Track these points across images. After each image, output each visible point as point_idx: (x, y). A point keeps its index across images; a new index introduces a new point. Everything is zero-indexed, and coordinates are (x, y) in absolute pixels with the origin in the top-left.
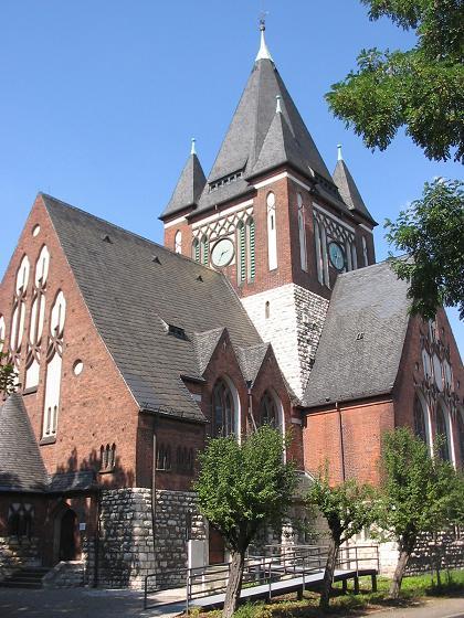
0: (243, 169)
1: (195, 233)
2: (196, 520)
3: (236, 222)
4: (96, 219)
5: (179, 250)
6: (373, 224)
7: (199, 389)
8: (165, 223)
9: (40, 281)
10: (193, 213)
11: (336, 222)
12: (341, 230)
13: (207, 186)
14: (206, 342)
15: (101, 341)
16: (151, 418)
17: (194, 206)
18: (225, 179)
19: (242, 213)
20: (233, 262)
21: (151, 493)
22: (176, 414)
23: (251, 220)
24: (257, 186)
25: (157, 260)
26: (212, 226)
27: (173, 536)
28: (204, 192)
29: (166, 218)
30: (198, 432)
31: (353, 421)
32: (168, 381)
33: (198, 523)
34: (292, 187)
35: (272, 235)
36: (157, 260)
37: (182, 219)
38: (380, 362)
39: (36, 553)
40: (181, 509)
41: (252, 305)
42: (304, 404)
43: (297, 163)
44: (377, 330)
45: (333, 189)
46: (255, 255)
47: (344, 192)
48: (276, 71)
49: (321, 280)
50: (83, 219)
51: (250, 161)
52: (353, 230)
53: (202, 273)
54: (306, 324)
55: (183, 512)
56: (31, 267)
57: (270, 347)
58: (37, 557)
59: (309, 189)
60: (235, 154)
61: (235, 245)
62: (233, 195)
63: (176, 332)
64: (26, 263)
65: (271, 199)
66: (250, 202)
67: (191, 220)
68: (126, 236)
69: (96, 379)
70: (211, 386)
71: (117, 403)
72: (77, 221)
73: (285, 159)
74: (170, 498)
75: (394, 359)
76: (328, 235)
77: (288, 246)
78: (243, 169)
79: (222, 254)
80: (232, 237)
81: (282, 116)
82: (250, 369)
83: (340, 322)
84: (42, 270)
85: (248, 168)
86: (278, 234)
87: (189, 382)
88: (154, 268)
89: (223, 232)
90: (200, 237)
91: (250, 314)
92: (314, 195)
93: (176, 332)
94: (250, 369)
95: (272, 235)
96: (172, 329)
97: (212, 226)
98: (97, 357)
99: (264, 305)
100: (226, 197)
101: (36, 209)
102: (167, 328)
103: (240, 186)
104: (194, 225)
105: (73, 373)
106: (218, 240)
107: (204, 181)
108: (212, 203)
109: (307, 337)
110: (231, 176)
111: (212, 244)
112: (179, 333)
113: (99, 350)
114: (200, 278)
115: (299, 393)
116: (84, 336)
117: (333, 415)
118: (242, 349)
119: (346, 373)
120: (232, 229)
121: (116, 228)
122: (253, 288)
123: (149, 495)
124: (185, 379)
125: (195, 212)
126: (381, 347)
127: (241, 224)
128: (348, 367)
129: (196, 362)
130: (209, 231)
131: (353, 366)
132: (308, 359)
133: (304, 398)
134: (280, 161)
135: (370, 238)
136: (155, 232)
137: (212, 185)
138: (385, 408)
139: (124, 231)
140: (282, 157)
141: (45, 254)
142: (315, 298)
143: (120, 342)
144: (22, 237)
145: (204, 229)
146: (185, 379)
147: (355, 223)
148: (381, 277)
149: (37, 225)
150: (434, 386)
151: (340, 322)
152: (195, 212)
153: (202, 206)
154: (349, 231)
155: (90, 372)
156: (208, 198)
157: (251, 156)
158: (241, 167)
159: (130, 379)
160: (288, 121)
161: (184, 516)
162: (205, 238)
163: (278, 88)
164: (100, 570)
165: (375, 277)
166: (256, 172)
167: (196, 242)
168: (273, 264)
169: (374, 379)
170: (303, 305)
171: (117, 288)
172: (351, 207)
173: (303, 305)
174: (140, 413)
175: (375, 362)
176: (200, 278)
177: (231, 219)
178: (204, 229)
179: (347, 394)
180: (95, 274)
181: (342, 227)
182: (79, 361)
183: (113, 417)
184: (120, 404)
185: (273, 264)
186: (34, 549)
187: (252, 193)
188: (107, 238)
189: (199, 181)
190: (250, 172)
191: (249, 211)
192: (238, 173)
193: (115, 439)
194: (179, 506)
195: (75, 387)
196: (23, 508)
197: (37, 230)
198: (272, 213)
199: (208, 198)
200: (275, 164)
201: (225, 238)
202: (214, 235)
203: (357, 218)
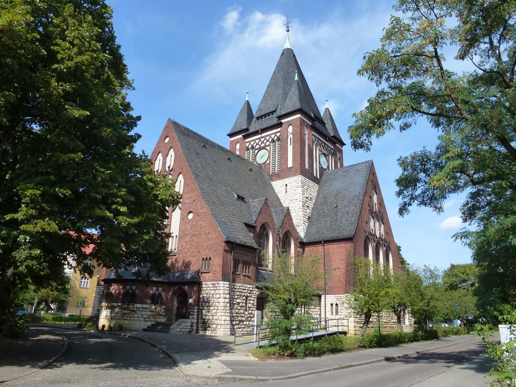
0: (275, 111)
1: (247, 144)
2: (250, 300)
3: (270, 140)
4: (198, 135)
5: (238, 153)
6: (343, 144)
7: (252, 230)
8: (230, 138)
9: (169, 167)
10: (247, 133)
11: (324, 143)
12: (329, 149)
13: (255, 119)
14: (256, 204)
15: (203, 202)
16: (230, 245)
17: (247, 130)
18: (265, 116)
19: (274, 135)
20: (268, 162)
21: (229, 285)
22: (243, 243)
23: (279, 139)
24: (283, 121)
25: (229, 159)
26: (257, 141)
27: (239, 308)
28: (253, 122)
29: (231, 135)
30: (253, 253)
31: (331, 251)
32: (238, 225)
33: (252, 302)
34: (302, 122)
35: (290, 148)
36: (229, 159)
37: (240, 136)
38: (347, 220)
39: (163, 314)
40: (243, 294)
41: (278, 185)
42: (304, 241)
43: (306, 109)
44: (345, 203)
45: (323, 124)
46: (281, 159)
47: (329, 126)
48: (294, 55)
49: (315, 175)
50: (192, 135)
51: (279, 107)
52: (332, 147)
53: (252, 167)
54: (307, 198)
55: (244, 296)
56: (163, 159)
57: (288, 209)
58: (164, 316)
59: (311, 124)
60: (271, 102)
61: (269, 152)
62: (269, 125)
63: (241, 198)
64: (160, 156)
65: (290, 129)
66: (279, 129)
67: (245, 137)
68: (213, 145)
69: (201, 222)
70: (258, 229)
71: (213, 236)
72: (189, 136)
73: (300, 107)
74: (238, 287)
75: (354, 219)
76: (320, 150)
77: (299, 155)
78: (275, 111)
79: (262, 157)
80: (268, 148)
81: (298, 82)
82: (277, 220)
83: (325, 198)
84: (170, 161)
85: (278, 110)
86: (294, 147)
87: (250, 227)
88: (228, 163)
89: (263, 145)
90: (250, 146)
91: (276, 190)
92: (313, 128)
93: (241, 198)
94: (277, 220)
95: (290, 148)
96: (239, 197)
97: (257, 141)
98: (202, 211)
99: (285, 186)
100: (265, 126)
101: (166, 128)
102: (236, 196)
103: (273, 120)
104: (247, 140)
105: (187, 218)
106: (260, 149)
107: (252, 116)
108: (257, 129)
109: (307, 205)
110: (268, 114)
111: (256, 151)
112: (242, 199)
113: (203, 207)
114: (251, 170)
115: (302, 234)
116: (194, 198)
117: (320, 248)
118: (273, 210)
119: (328, 225)
120: (268, 143)
121: (208, 140)
122: (279, 176)
123: (228, 286)
124: (247, 225)
125: (247, 133)
126: (348, 212)
127: (273, 141)
128: (329, 222)
129: (251, 215)
130: (255, 144)
131: (332, 221)
132: (307, 217)
133: (305, 237)
134: (297, 108)
135: (341, 151)
136: (225, 142)
137: (258, 118)
138: (348, 245)
139: (212, 142)
140: (297, 105)
141: (172, 152)
142: (311, 183)
143: (214, 204)
144: (159, 143)
145: (252, 143)
146: (247, 225)
147: (334, 143)
148: (348, 174)
149: (167, 137)
150: (375, 235)
151: (325, 198)
152: (247, 133)
153: (251, 130)
154: (330, 148)
155: (197, 218)
156: (255, 126)
157: (280, 104)
158: (274, 109)
159: (220, 223)
160: (301, 85)
161: (244, 298)
162: (253, 147)
163: (295, 65)
164: (200, 325)
165: (345, 174)
166: (283, 113)
167: (248, 149)
168: (290, 164)
169: (344, 229)
170: (306, 187)
171: (211, 173)
172: (332, 134)
173: (306, 187)
174: (226, 242)
175: (344, 220)
176: (251, 170)
177: (267, 138)
178: (252, 143)
179: (329, 235)
180: (199, 165)
181: (327, 145)
182: (191, 212)
183: (210, 243)
184: (214, 237)
185: (290, 164)
186: (163, 312)
187: (280, 125)
188: (204, 146)
189: (250, 116)
190: (279, 113)
191: (278, 134)
192: (272, 113)
193: (211, 255)
194: (243, 292)
195: (188, 226)
196: (131, 289)
197: (167, 140)
198: (291, 136)
199: (255, 126)
200: (293, 109)
201: (264, 148)
202: (258, 147)
203: (335, 140)
